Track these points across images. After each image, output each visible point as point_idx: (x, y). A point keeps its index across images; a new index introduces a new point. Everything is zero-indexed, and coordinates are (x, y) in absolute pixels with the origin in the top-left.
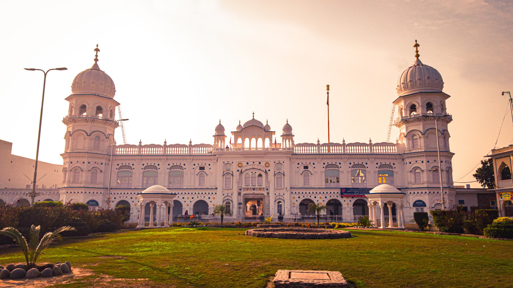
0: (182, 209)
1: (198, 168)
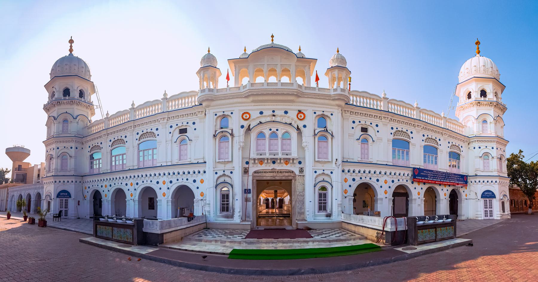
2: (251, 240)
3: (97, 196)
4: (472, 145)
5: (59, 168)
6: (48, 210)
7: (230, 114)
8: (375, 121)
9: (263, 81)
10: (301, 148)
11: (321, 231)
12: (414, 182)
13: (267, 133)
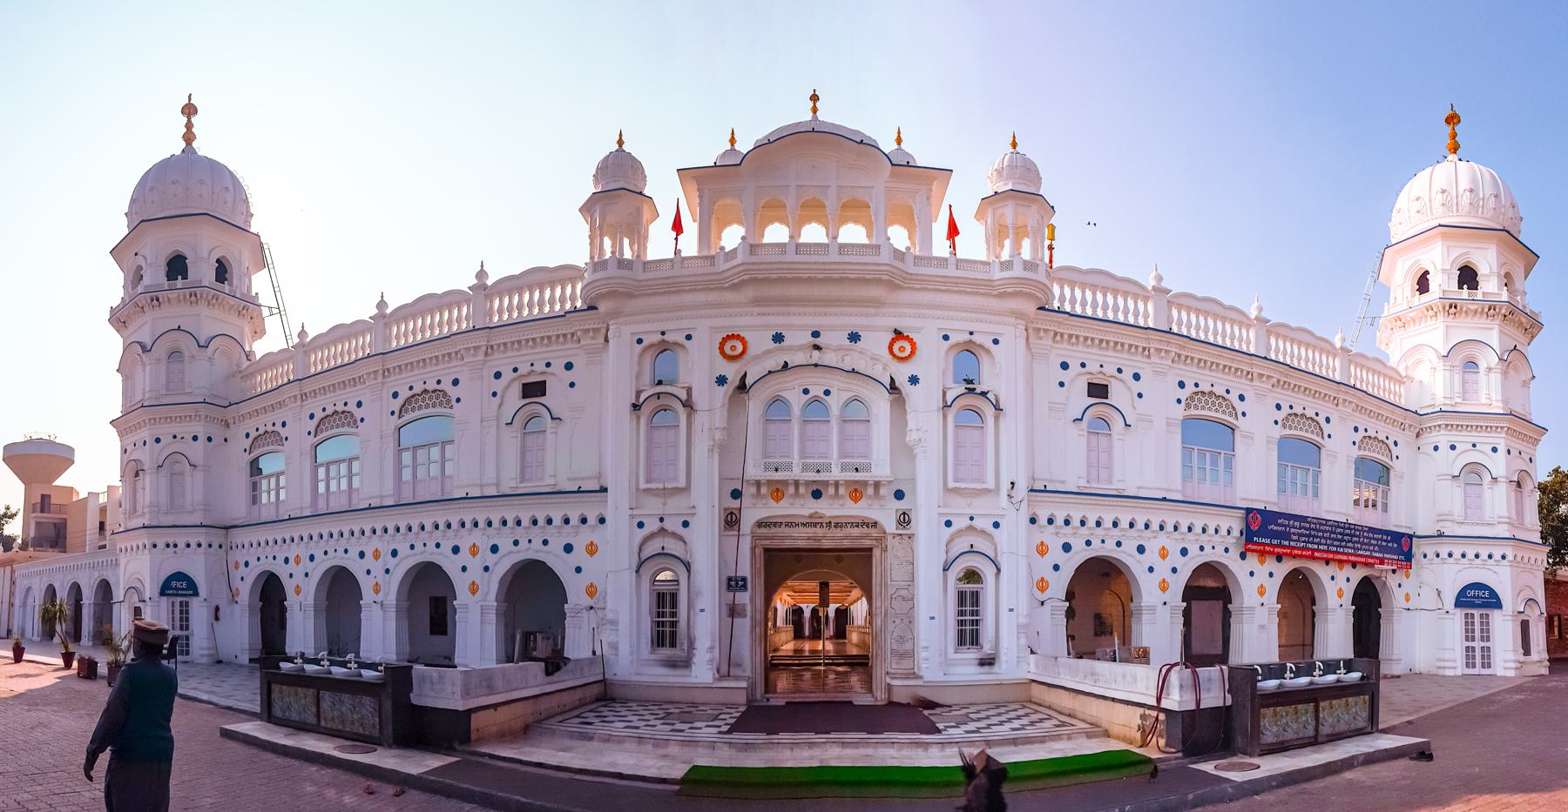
0: (359, 607)
1: (516, 389)
3: (271, 592)
4: (1430, 439)
5: (164, 500)
7: (682, 340)
8: (1132, 363)
9: (786, 240)
10: (903, 449)
12: (1249, 554)
13: (796, 400)
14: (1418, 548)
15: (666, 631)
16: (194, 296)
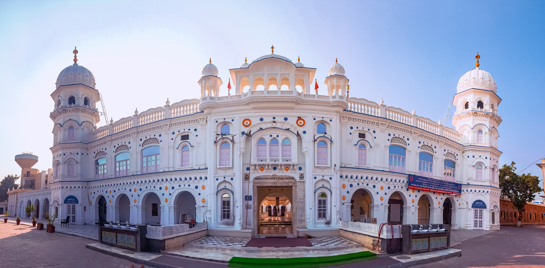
1: (179, 137)
2: (252, 248)
3: (102, 202)
4: (466, 154)
5: (66, 173)
6: (56, 215)
7: (230, 121)
9: (263, 90)
11: (320, 239)
13: (268, 139)
14: (463, 188)
15: (226, 213)
16: (77, 109)
